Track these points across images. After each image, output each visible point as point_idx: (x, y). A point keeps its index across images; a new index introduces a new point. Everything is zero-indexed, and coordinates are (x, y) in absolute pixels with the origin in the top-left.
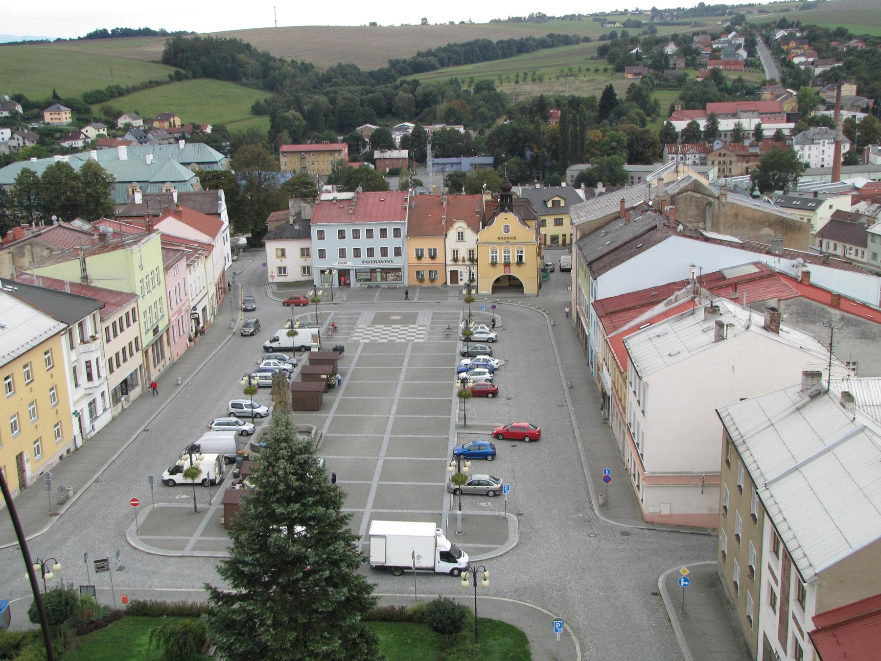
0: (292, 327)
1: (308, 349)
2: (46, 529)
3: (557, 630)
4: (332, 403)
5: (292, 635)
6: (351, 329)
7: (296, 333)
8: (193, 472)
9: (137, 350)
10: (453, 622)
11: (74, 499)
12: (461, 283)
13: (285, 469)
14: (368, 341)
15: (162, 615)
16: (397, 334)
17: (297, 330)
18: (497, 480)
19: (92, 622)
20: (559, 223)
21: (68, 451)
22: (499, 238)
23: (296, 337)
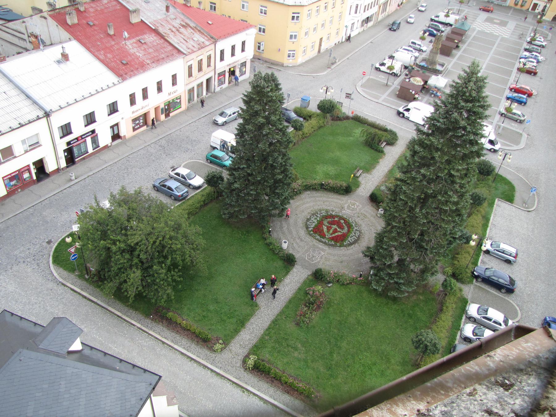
0: (448, 13)
1: (451, 25)
2: (325, 73)
3: (532, 191)
4: (456, 55)
5: (446, 158)
6: (474, 21)
7: (449, 16)
8: (391, 68)
9: (377, 4)
10: (488, 171)
11: (338, 64)
12: (536, 11)
13: (472, 87)
14: (480, 29)
15: (365, 124)
16: (492, 29)
17: (450, 15)
18: (524, 116)
19: (338, 117)
21: (339, 42)
23: (448, 18)
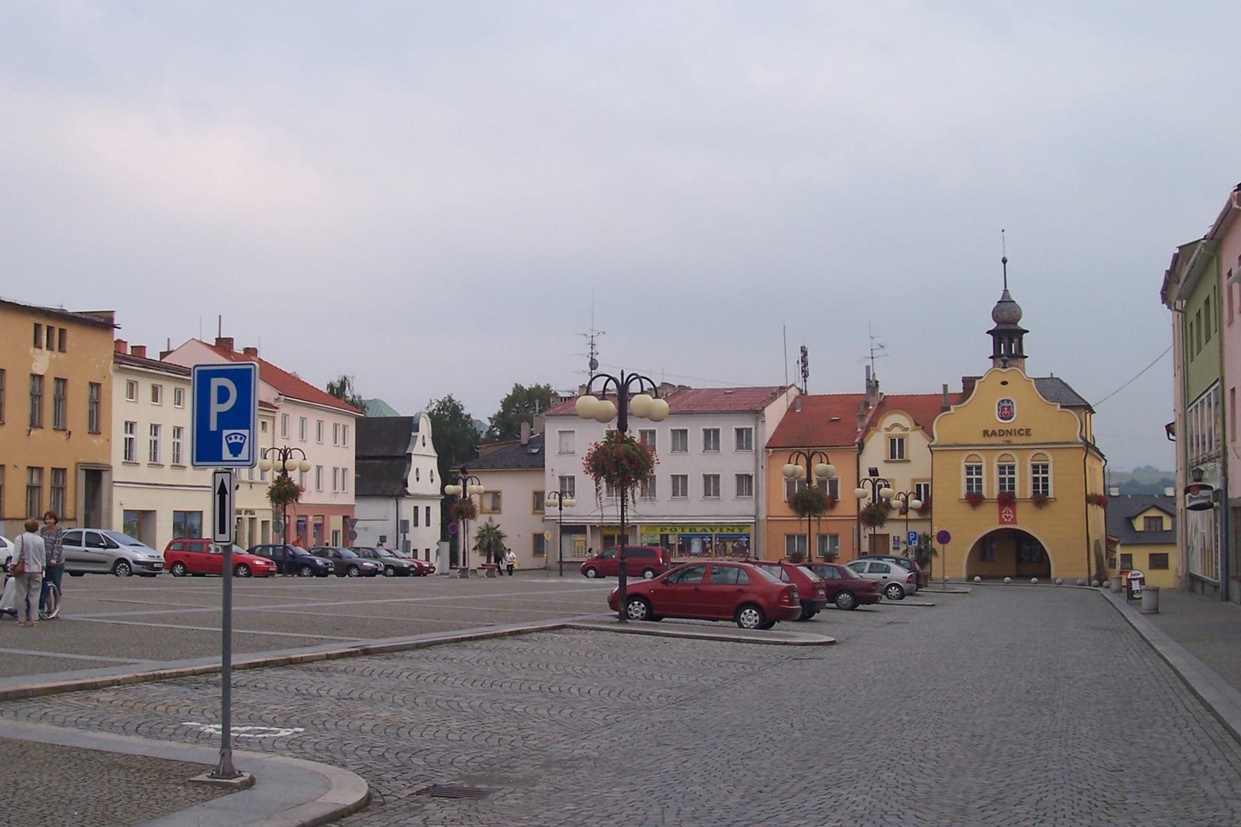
20: (1159, 562)
22: (986, 433)
